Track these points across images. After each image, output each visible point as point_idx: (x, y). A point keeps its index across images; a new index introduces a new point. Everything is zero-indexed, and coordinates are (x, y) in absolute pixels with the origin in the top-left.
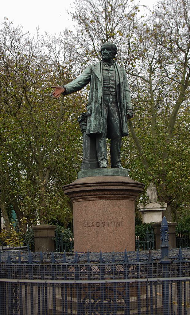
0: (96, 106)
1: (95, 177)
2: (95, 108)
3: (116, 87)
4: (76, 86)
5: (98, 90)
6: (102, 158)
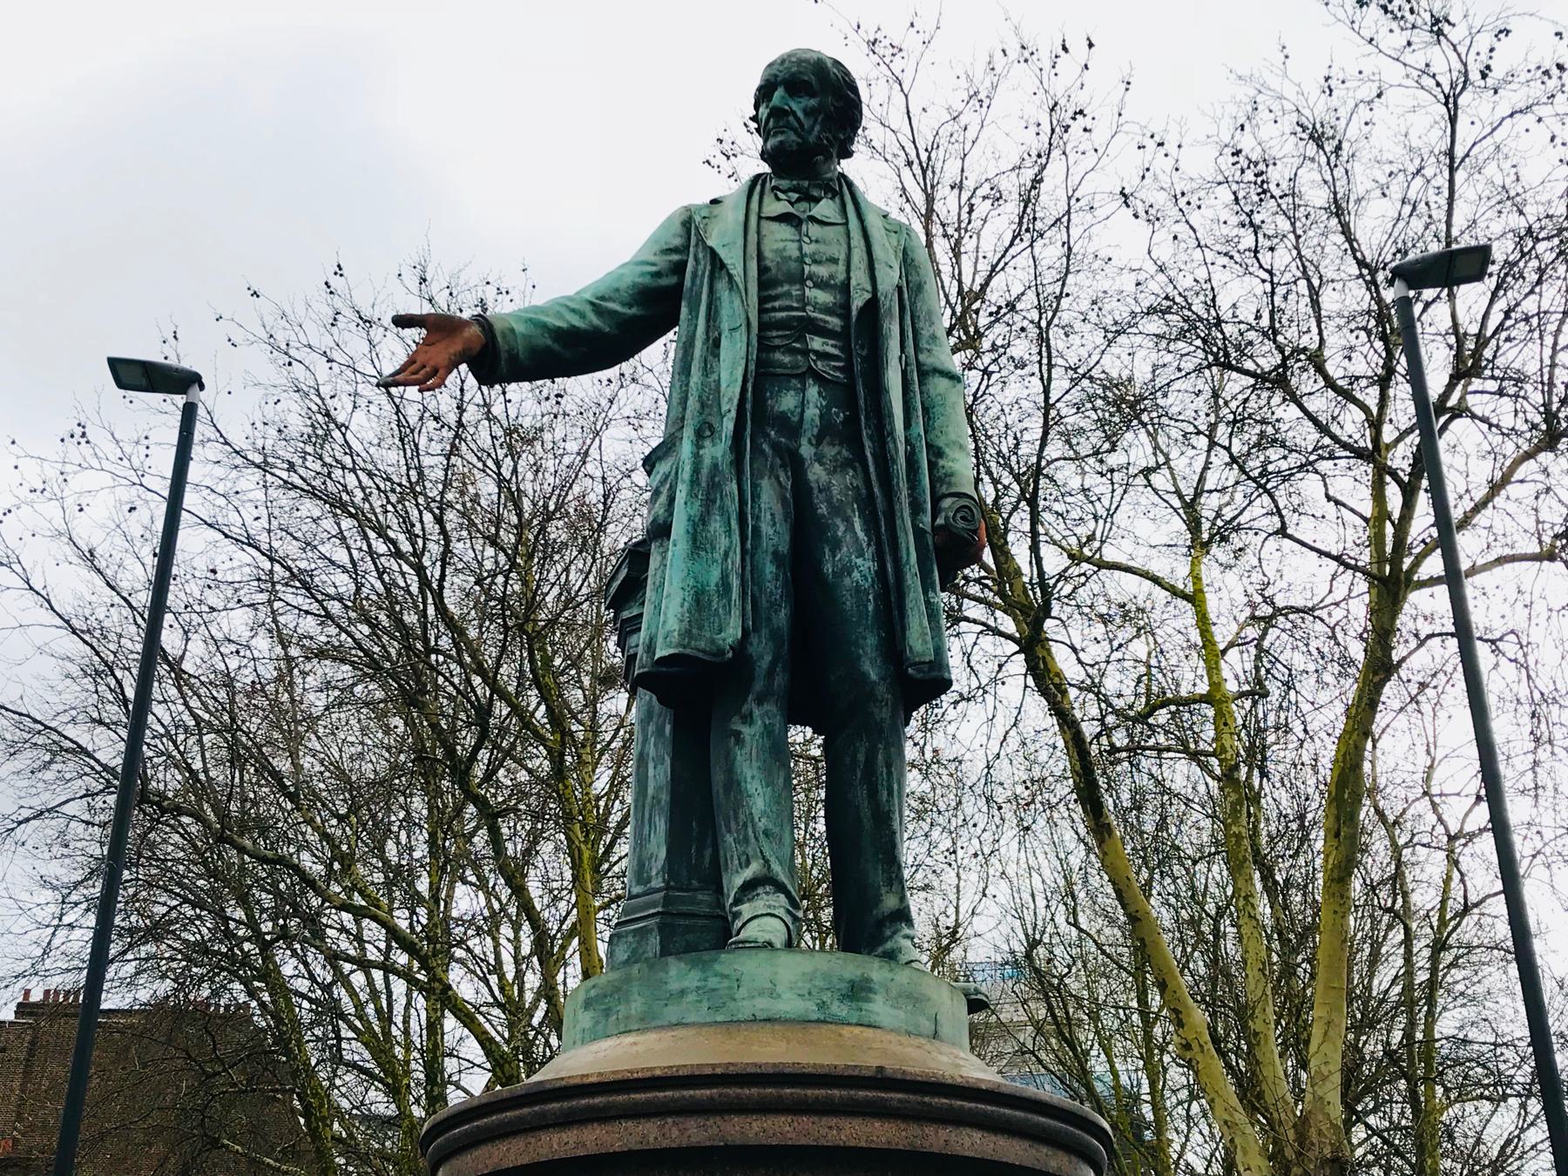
0: (707, 462)
1: (668, 1035)
2: (696, 471)
3: (846, 327)
4: (576, 321)
5: (724, 343)
6: (748, 874)
